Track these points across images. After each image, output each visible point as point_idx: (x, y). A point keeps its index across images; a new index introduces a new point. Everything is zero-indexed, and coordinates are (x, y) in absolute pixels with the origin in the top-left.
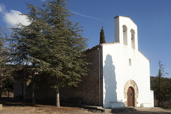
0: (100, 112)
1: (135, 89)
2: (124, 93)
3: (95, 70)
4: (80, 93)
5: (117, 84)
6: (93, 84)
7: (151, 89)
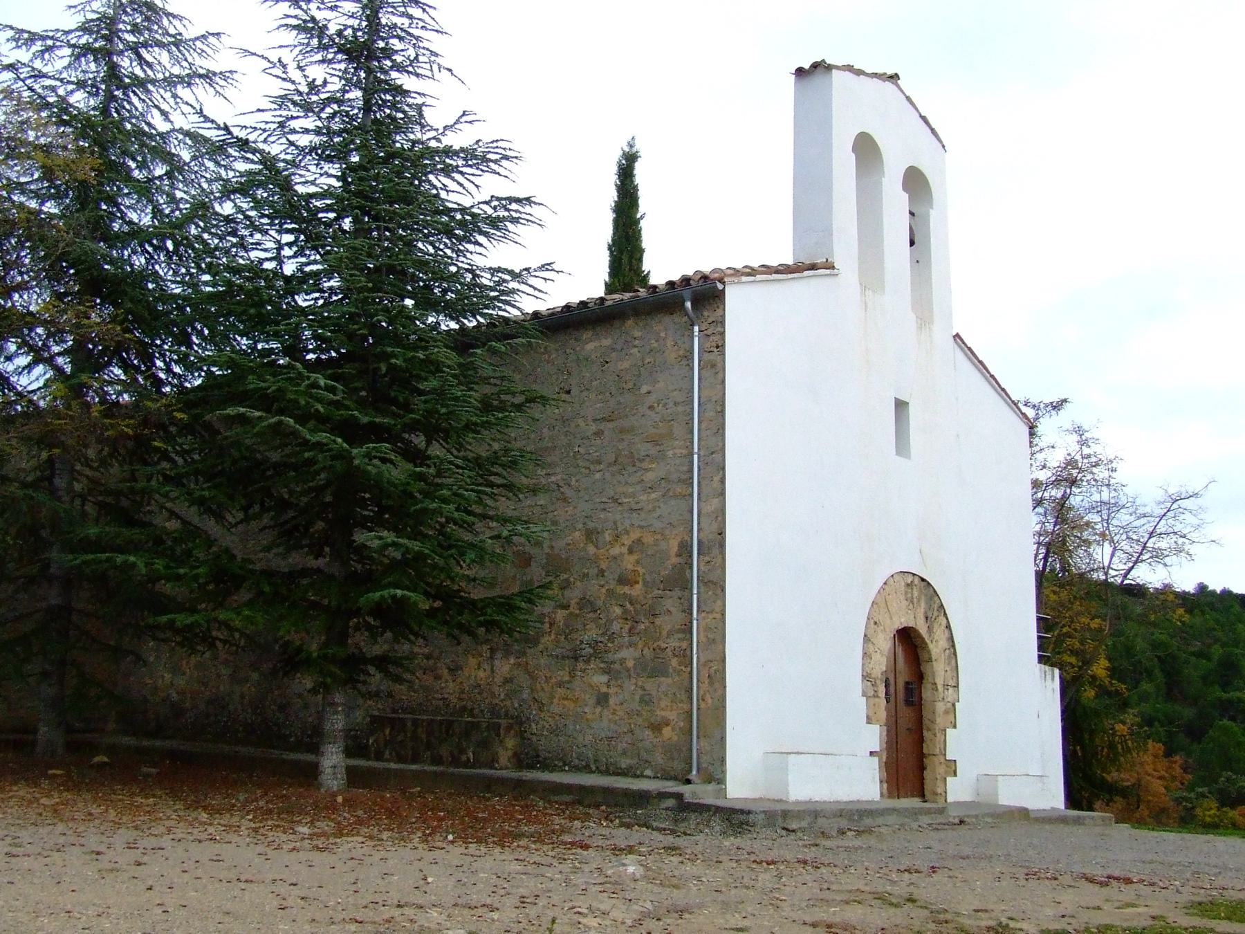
0: (717, 824)
1: (936, 647)
2: (866, 677)
3: (650, 476)
4: (504, 667)
5: (1231, 589)
6: (637, 591)
7: (1041, 659)
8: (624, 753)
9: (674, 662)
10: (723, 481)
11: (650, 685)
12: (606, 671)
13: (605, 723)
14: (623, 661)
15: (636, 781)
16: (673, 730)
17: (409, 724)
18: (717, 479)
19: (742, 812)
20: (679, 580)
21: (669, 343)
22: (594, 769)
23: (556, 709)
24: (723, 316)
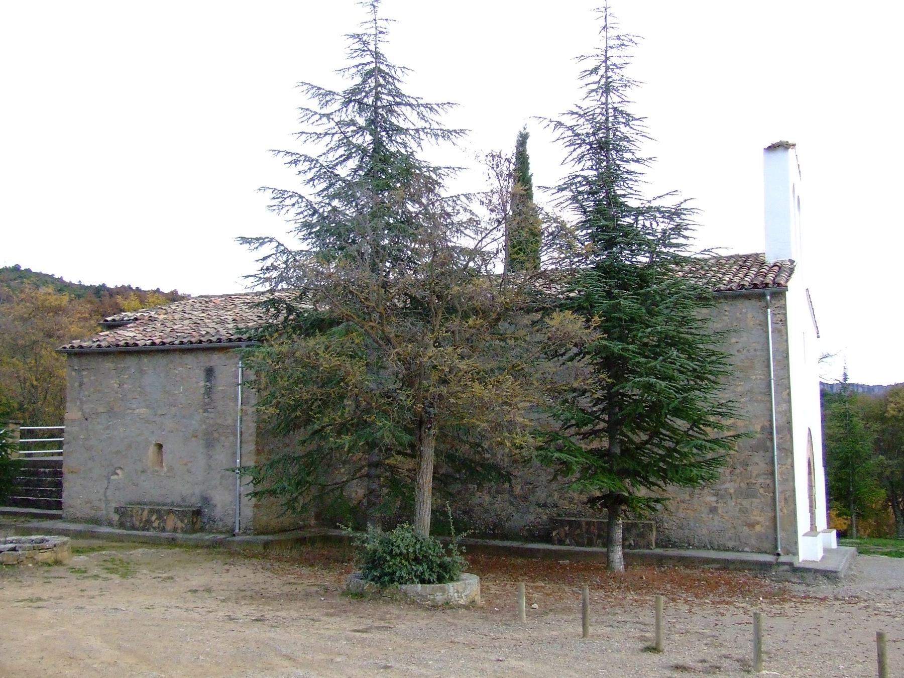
8: (730, 539)
9: (761, 491)
10: (789, 394)
11: (746, 503)
12: (716, 495)
13: (716, 523)
14: (726, 490)
15: (739, 554)
16: (762, 526)
17: (584, 524)
18: (785, 393)
19: (832, 572)
20: (765, 446)
21: (749, 316)
22: (710, 547)
23: (681, 514)
24: (785, 305)
